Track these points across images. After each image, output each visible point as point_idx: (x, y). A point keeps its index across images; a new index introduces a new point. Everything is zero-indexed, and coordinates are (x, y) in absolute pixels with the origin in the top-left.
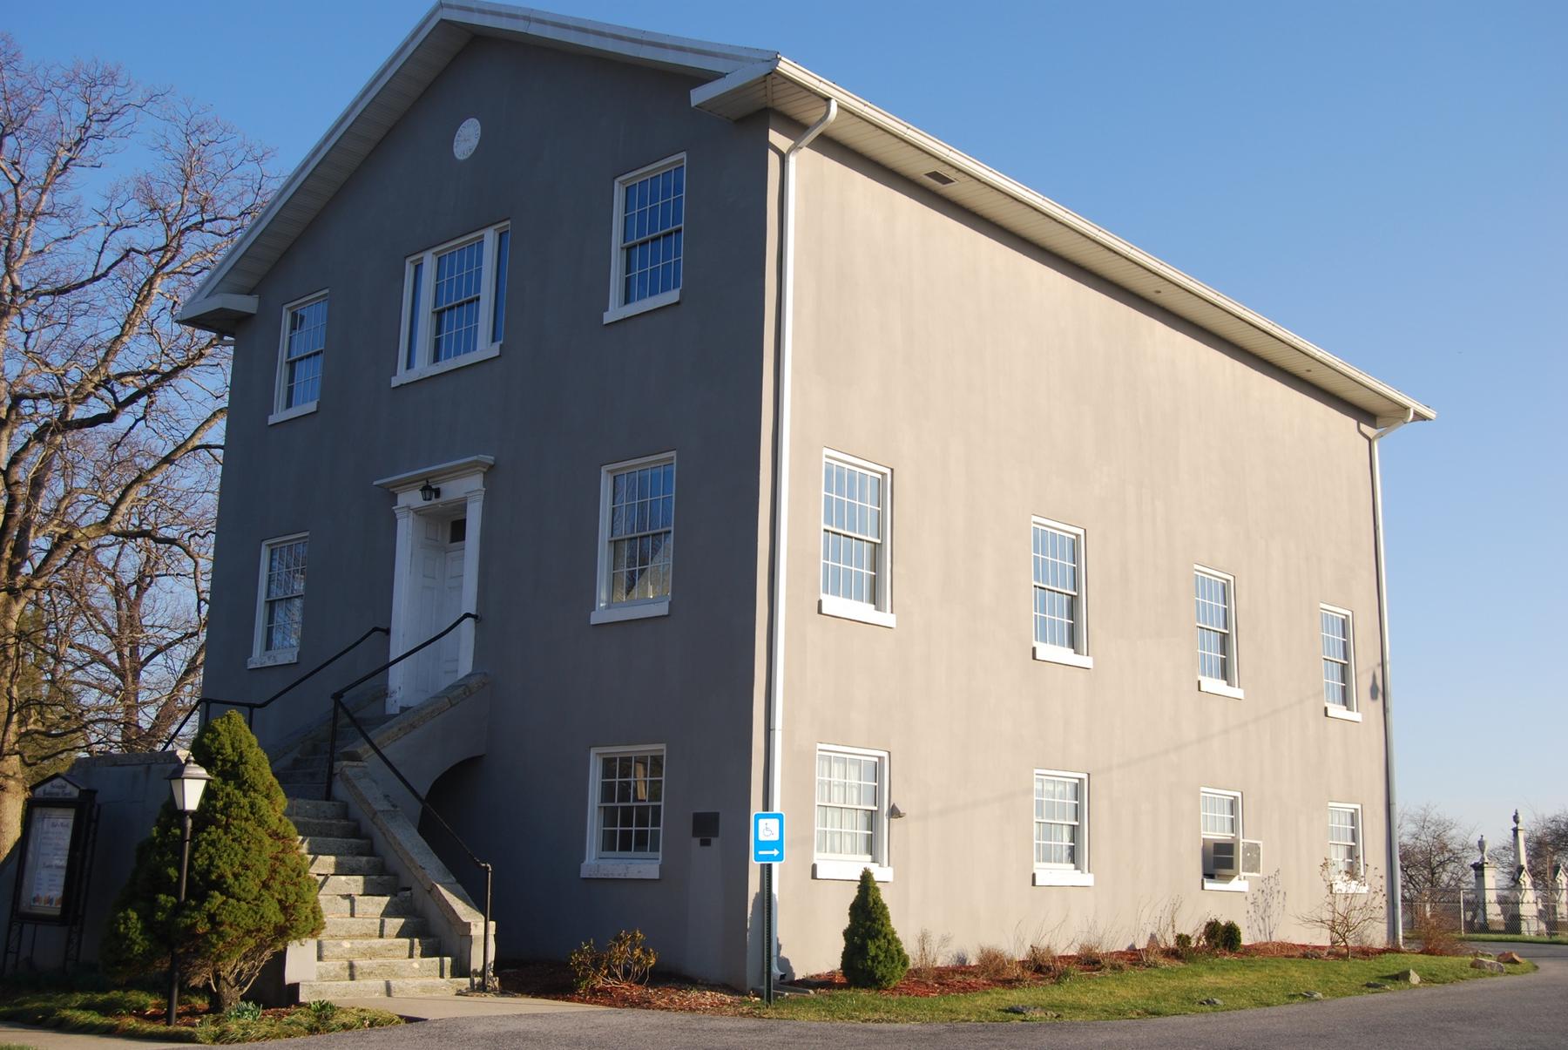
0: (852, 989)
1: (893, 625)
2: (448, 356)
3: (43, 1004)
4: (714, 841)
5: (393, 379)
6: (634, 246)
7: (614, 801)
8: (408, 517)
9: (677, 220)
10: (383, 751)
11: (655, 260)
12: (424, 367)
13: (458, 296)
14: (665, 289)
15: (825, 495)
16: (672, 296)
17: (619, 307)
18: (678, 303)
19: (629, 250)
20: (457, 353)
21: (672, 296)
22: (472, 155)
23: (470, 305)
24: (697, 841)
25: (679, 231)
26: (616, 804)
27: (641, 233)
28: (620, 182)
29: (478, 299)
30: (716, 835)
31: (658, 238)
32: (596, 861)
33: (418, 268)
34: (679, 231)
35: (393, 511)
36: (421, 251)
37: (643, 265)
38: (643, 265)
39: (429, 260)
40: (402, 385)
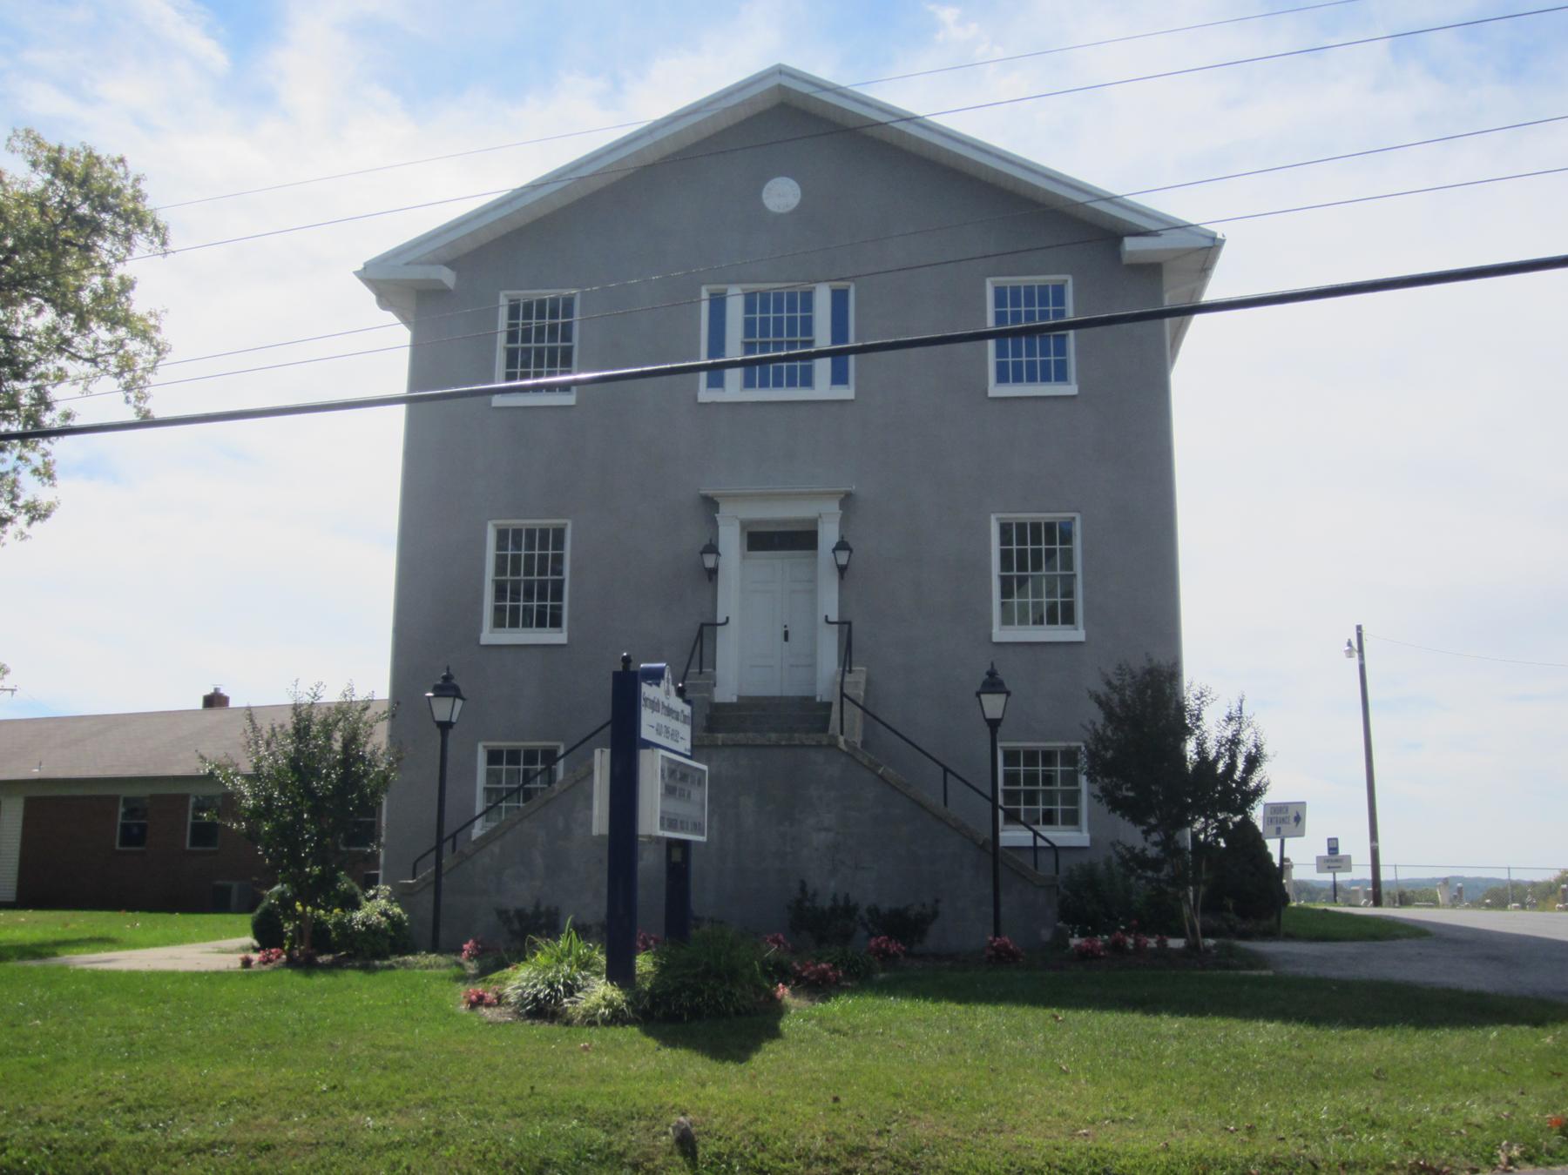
18: (852, 400)
35: (715, 518)
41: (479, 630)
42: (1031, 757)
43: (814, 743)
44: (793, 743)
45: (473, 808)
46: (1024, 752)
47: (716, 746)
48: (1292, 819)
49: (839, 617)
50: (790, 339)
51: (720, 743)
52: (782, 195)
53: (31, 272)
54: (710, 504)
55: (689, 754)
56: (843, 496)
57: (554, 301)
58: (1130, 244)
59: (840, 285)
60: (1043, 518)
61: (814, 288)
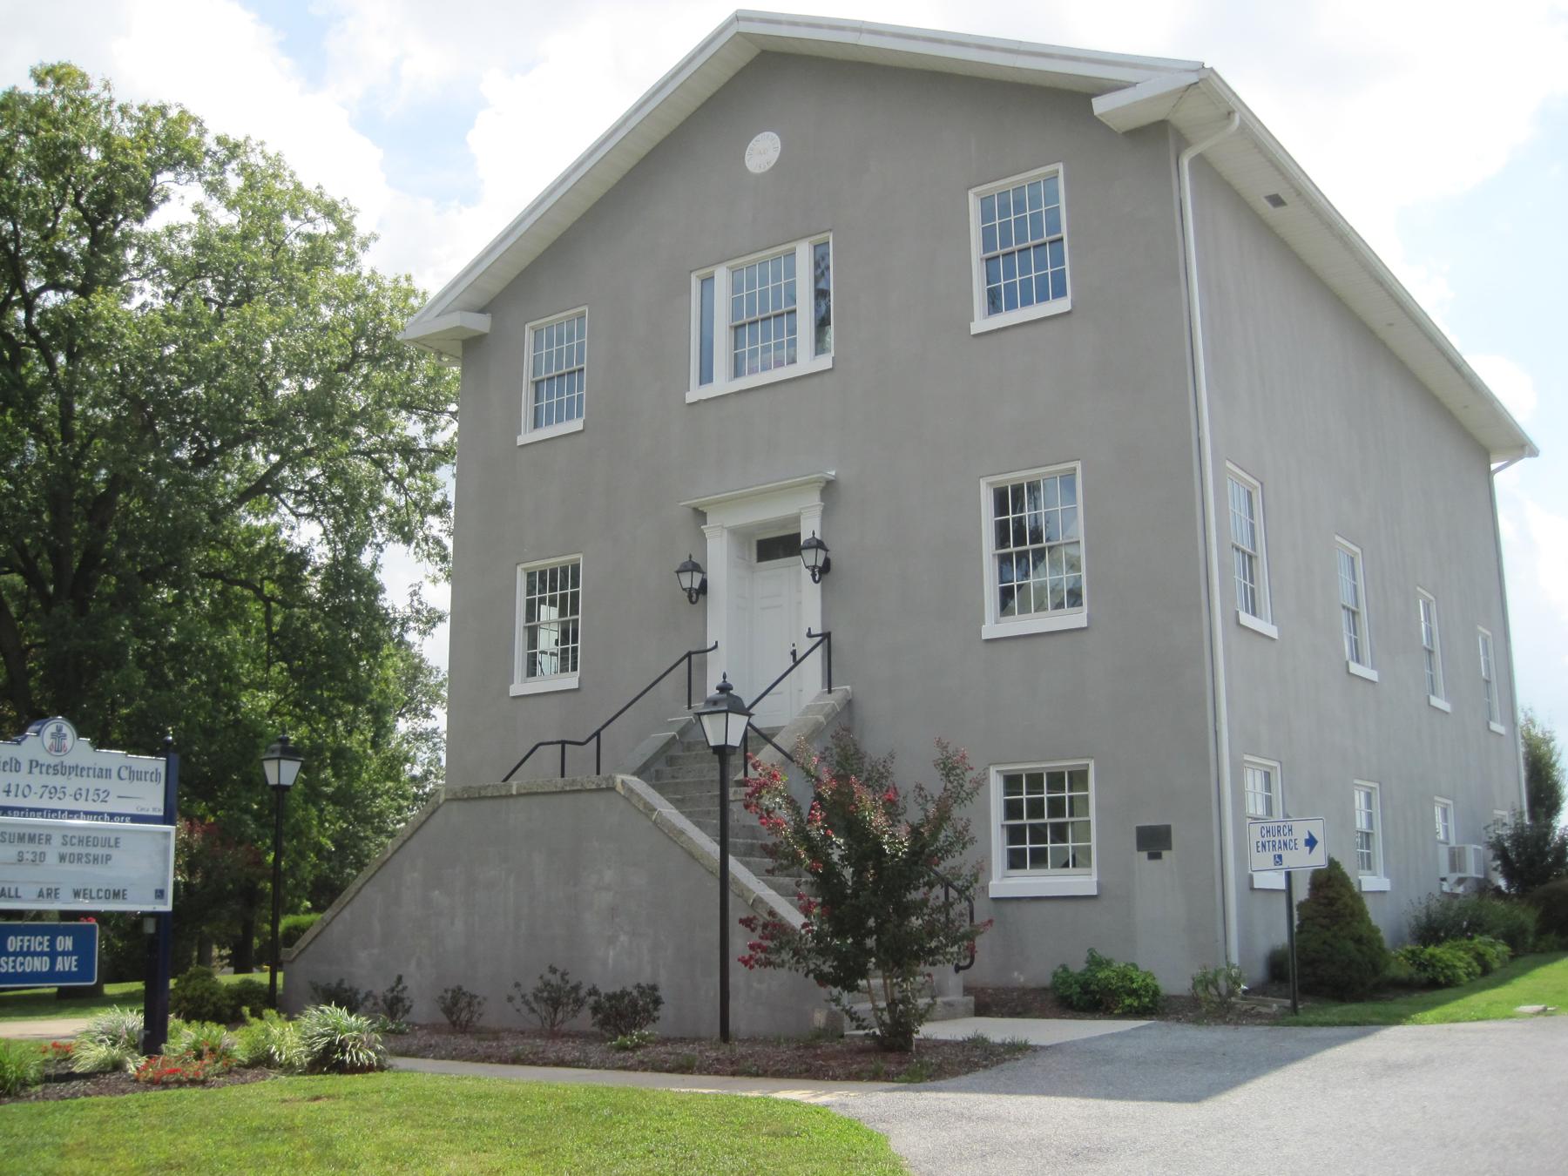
0: (839, 988)
1: (1275, 636)
2: (549, 423)
3: (750, 1095)
4: (1165, 854)
5: (687, 394)
6: (543, 381)
7: (1022, 818)
8: (721, 536)
9: (580, 361)
10: (717, 777)
11: (560, 393)
12: (722, 383)
13: (559, 367)
14: (570, 417)
15: (1031, 543)
16: (576, 425)
17: (730, 380)
18: (1068, 313)
19: (537, 384)
20: (560, 420)
21: (1062, 305)
22: (769, 170)
23: (765, 323)
24: (1144, 854)
25: (581, 370)
26: (1046, 820)
27: (559, 367)
28: (975, 194)
29: (794, 311)
30: (1169, 848)
31: (563, 375)
32: (1004, 882)
33: (707, 281)
34: (581, 370)
35: (702, 531)
36: (795, 240)
37: (550, 396)
38: (550, 396)
39: (722, 276)
40: (700, 401)
41: (981, 621)
42: (1035, 781)
43: (594, 787)
44: (575, 788)
45: (692, 856)
46: (1048, 774)
47: (512, 796)
48: (1301, 843)
49: (823, 627)
50: (569, 370)
51: (514, 792)
52: (763, 152)
53: (382, 338)
54: (700, 515)
55: (1246, 765)
56: (822, 485)
57: (1019, 190)
58: (1100, 105)
59: (818, 238)
60: (1008, 481)
61: (713, 272)
